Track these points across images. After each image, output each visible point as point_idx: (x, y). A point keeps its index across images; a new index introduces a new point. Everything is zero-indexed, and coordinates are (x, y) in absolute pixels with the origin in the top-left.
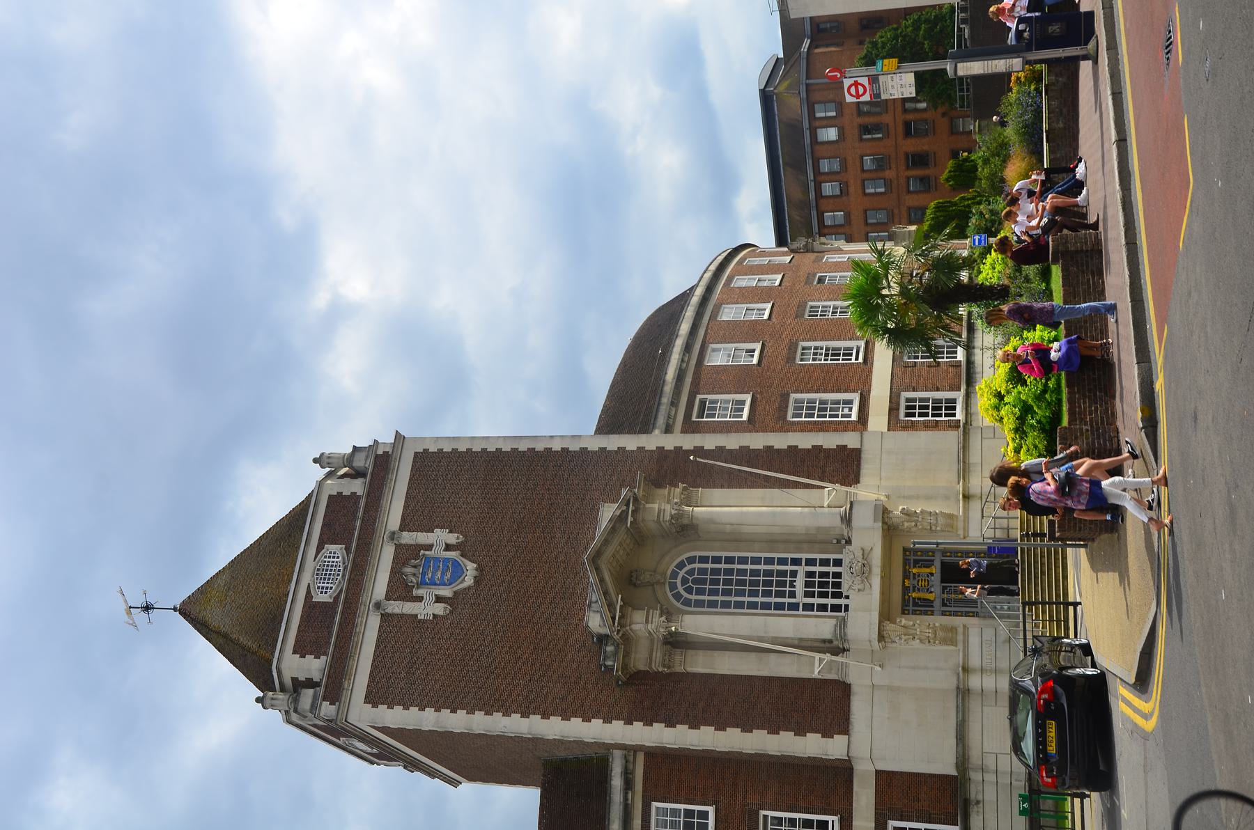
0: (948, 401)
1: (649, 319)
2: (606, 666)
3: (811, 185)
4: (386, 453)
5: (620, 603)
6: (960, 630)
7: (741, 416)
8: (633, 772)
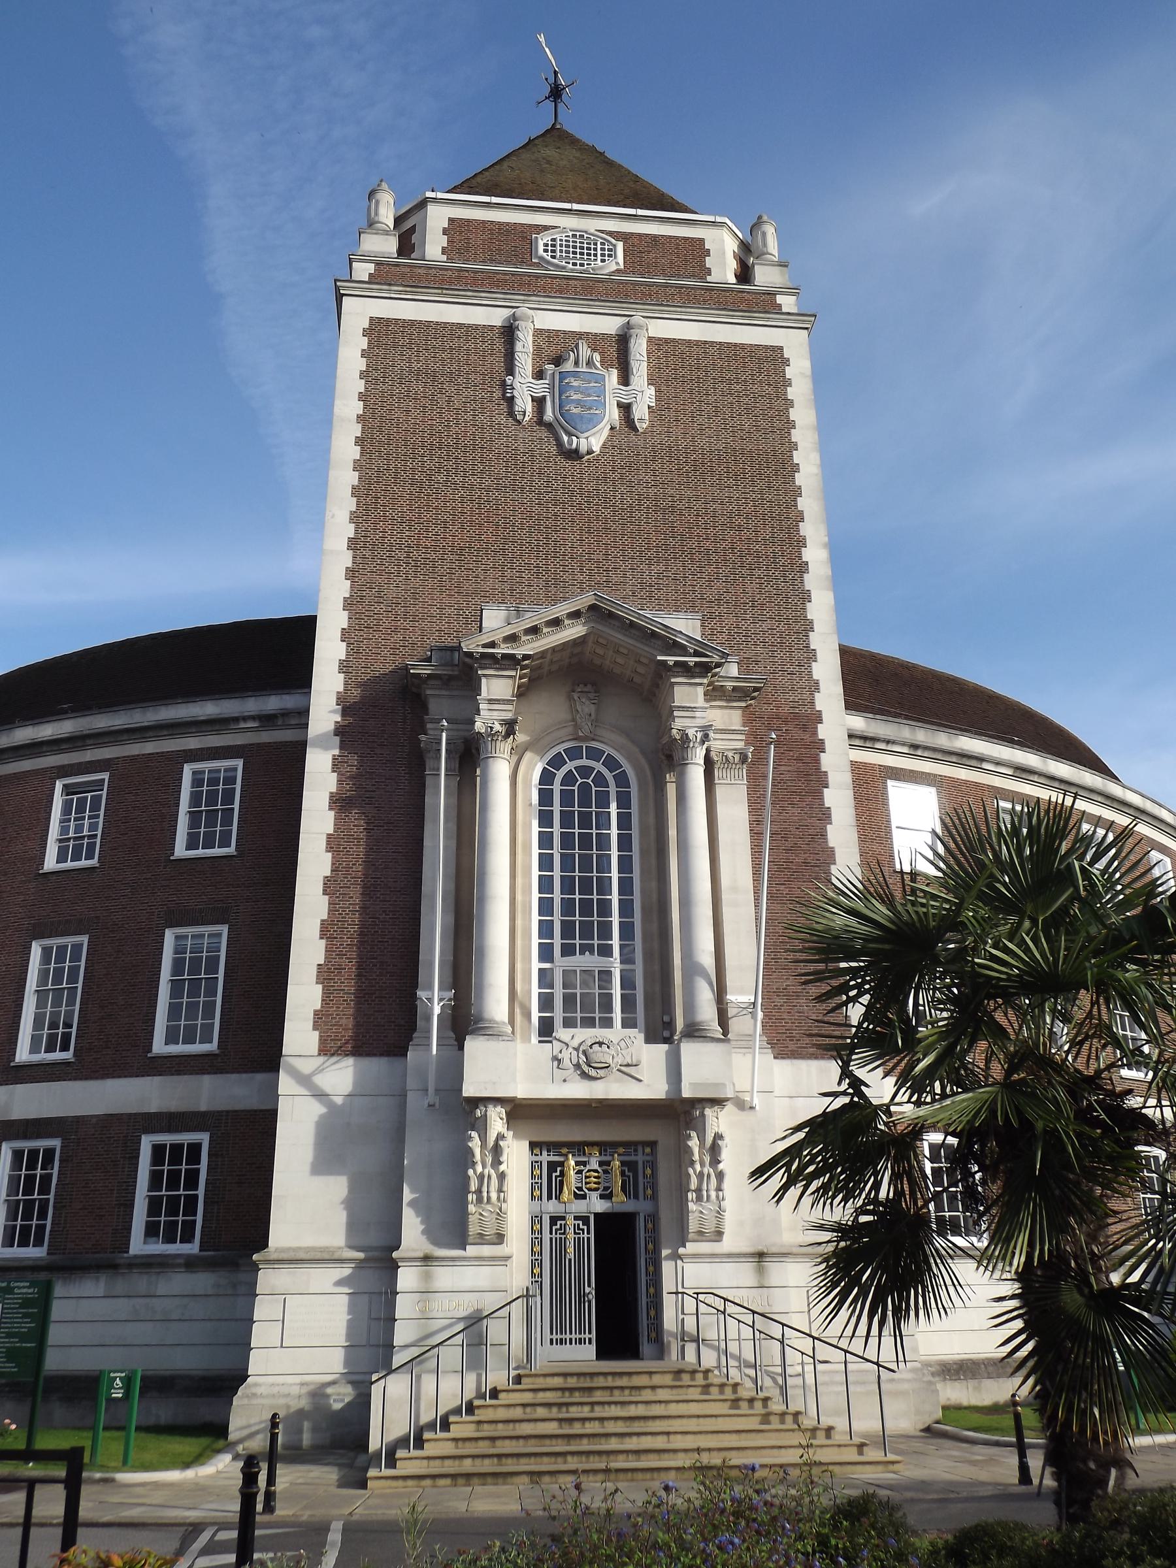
1: (1076, 739)
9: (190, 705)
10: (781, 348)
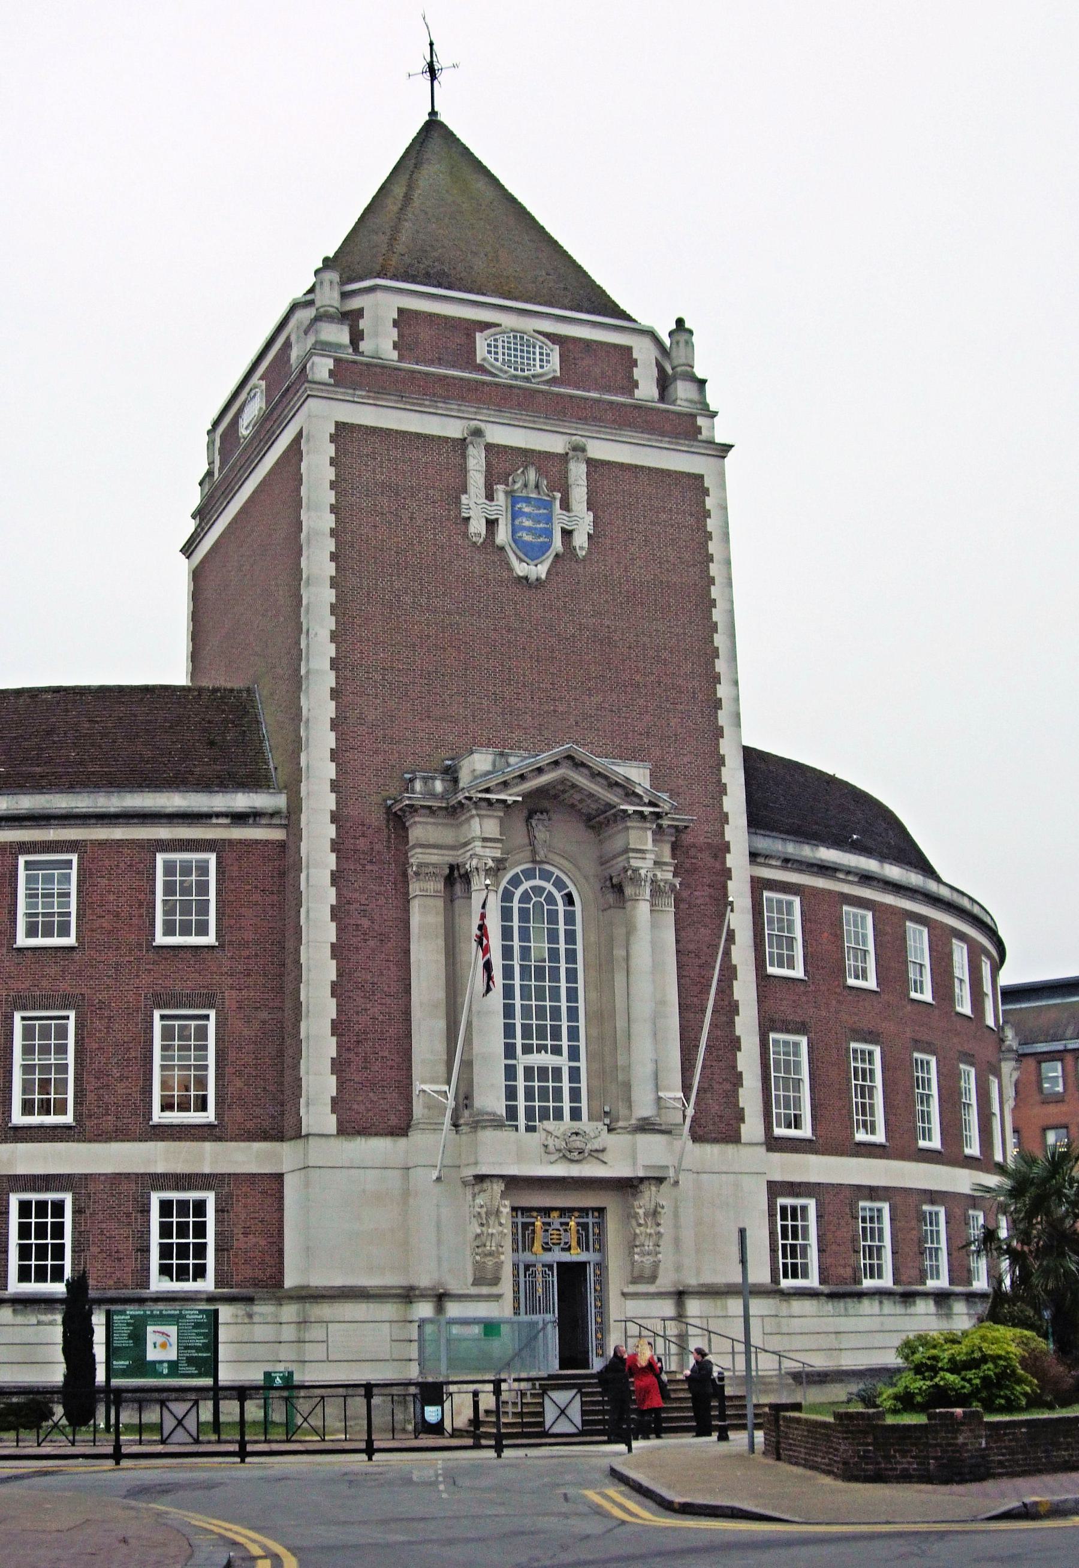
0: (805, 1266)
2: (411, 780)
3: (1058, 1046)
4: (699, 430)
5: (510, 799)
6: (494, 1290)
7: (772, 965)
8: (256, 825)
9: (158, 795)
10: (701, 477)
